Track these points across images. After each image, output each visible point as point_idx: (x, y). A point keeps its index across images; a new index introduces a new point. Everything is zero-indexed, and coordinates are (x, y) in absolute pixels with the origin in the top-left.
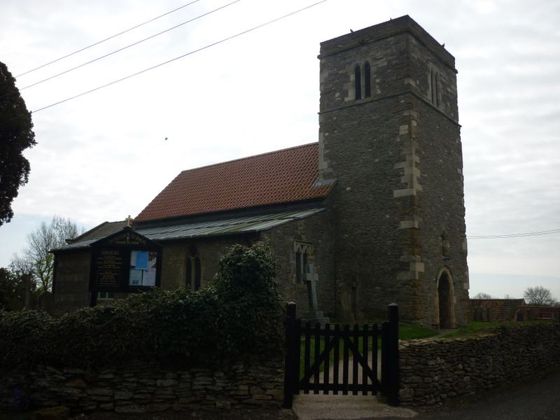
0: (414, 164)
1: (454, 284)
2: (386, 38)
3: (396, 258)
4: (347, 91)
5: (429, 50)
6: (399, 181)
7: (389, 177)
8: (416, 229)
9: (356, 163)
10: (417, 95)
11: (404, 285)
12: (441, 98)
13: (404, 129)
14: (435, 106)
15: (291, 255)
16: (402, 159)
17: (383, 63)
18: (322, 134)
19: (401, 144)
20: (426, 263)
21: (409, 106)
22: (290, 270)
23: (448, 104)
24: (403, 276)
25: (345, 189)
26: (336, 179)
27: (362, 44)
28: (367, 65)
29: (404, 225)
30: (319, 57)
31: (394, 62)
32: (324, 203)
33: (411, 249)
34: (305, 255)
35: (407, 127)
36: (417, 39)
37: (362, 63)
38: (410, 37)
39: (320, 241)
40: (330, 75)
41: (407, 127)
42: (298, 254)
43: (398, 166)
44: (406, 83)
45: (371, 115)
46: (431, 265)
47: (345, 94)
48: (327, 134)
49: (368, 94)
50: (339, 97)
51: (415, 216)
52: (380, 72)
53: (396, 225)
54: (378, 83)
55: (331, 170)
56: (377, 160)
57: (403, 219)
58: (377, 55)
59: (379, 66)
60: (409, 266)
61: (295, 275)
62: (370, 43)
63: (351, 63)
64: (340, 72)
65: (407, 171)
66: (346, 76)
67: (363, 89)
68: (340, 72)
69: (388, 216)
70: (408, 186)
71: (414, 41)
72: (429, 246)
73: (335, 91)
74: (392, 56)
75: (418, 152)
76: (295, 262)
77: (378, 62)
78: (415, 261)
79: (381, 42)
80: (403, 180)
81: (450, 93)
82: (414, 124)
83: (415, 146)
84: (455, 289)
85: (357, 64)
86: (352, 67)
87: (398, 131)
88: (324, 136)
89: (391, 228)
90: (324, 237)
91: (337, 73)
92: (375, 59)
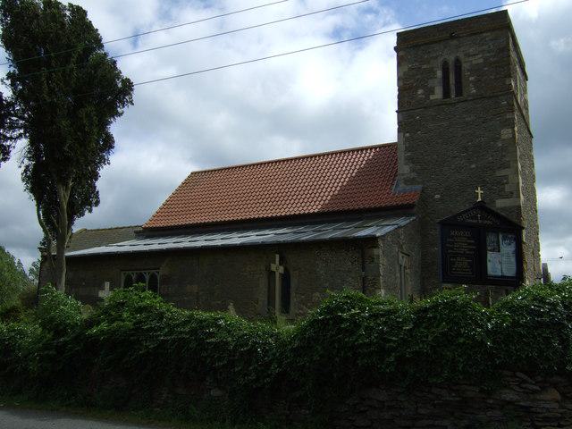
16: (506, 166)
17: (478, 60)
37: (451, 59)
47: (432, 91)
80: (507, 189)
92: (468, 55)
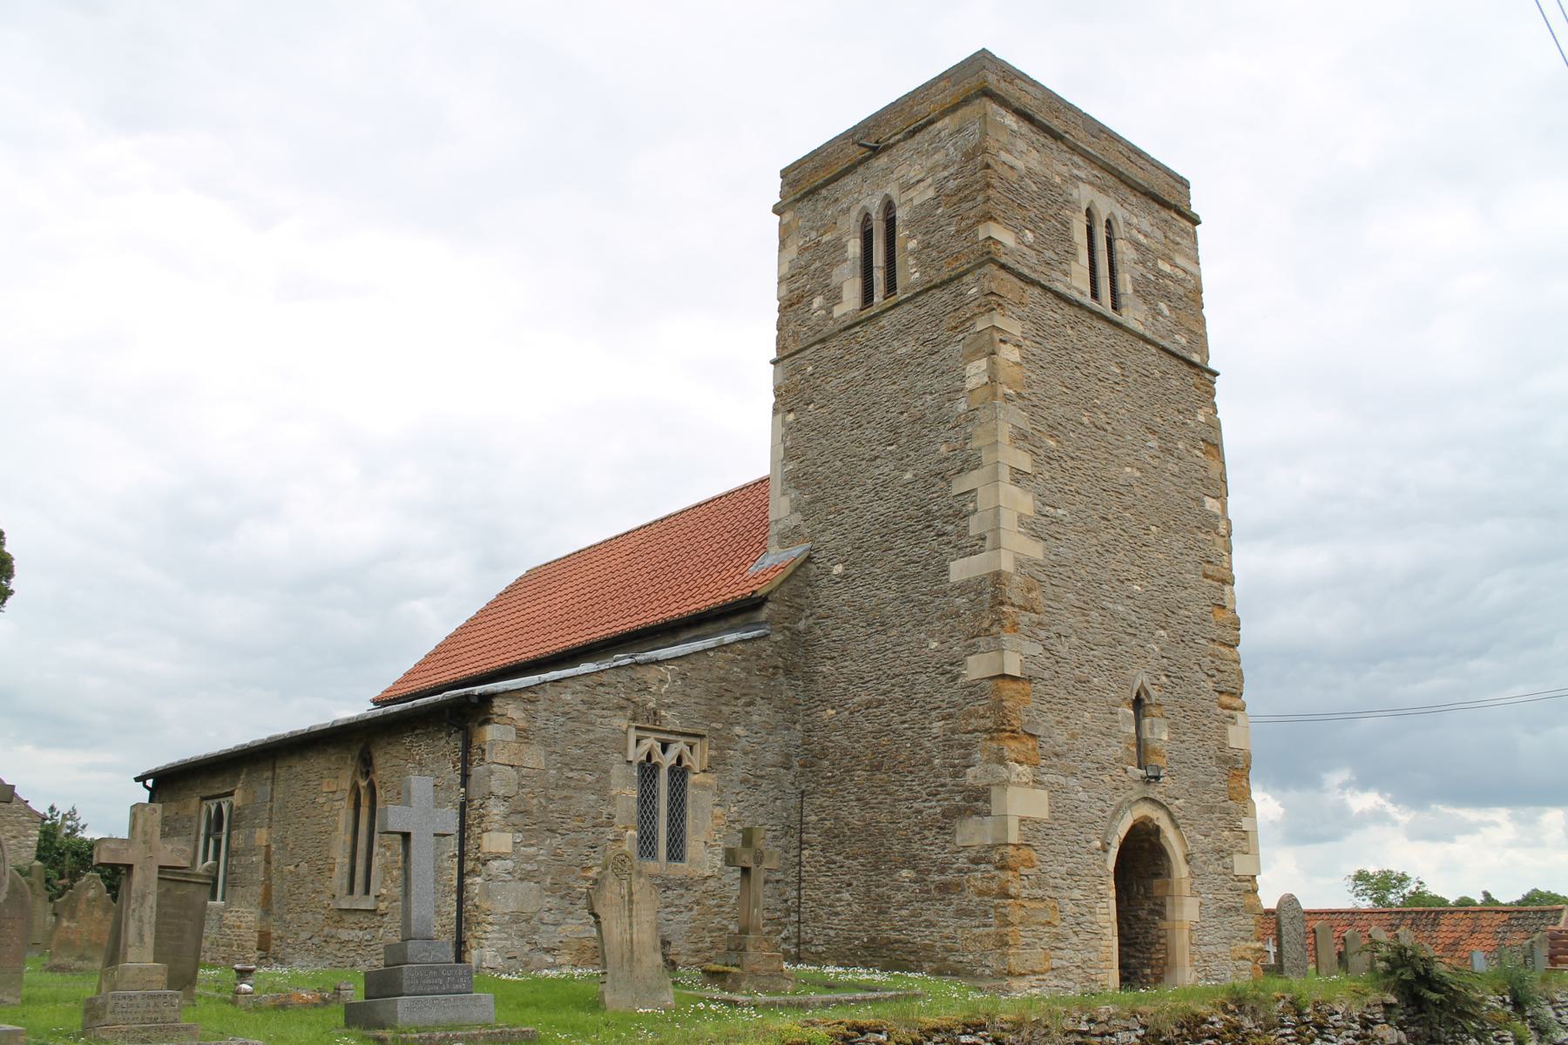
0: (1005, 474)
1: (1188, 858)
2: (931, 122)
3: (955, 775)
4: (841, 288)
5: (1074, 149)
6: (963, 533)
7: (938, 523)
8: (1014, 679)
9: (857, 491)
10: (1026, 271)
11: (976, 861)
12: (1130, 290)
13: (976, 372)
14: (1110, 313)
15: (617, 771)
16: (970, 463)
18: (779, 416)
19: (971, 416)
20: (1055, 791)
21: (992, 301)
22: (611, 817)
23: (1163, 306)
24: (973, 833)
25: (828, 572)
26: (809, 545)
27: (876, 151)
28: (889, 207)
29: (977, 668)
30: (778, 210)
31: (952, 184)
32: (764, 614)
33: (994, 745)
34: (679, 772)
35: (983, 363)
36: (1024, 115)
37: (875, 205)
38: (992, 107)
39: (738, 730)
40: (802, 250)
41: (983, 363)
42: (648, 770)
43: (960, 485)
44: (981, 237)
45: (896, 344)
46: (1082, 796)
47: (835, 297)
48: (791, 417)
49: (891, 286)
50: (821, 308)
51: (1005, 637)
52: (922, 219)
53: (956, 670)
54: (912, 253)
55: (796, 519)
56: (908, 476)
57: (972, 649)
58: (912, 174)
59: (916, 202)
60: (988, 801)
61: (633, 833)
62: (893, 145)
63: (849, 209)
64: (826, 238)
65: (983, 500)
66: (839, 246)
67: (879, 276)
68: (826, 238)
69: (934, 645)
70: (988, 544)
71: (1010, 121)
72: (1073, 736)
73: (812, 294)
74: (945, 167)
75: (1021, 437)
76: (633, 793)
77: (912, 193)
78: (1004, 784)
79: (918, 137)
80: (975, 526)
81: (1169, 276)
82: (1009, 354)
83: (1010, 419)
84: (1192, 874)
85: (864, 207)
86: (852, 223)
87: (963, 379)
88: (783, 421)
89: (943, 679)
90: (755, 718)
91: (818, 244)
92: (907, 187)
